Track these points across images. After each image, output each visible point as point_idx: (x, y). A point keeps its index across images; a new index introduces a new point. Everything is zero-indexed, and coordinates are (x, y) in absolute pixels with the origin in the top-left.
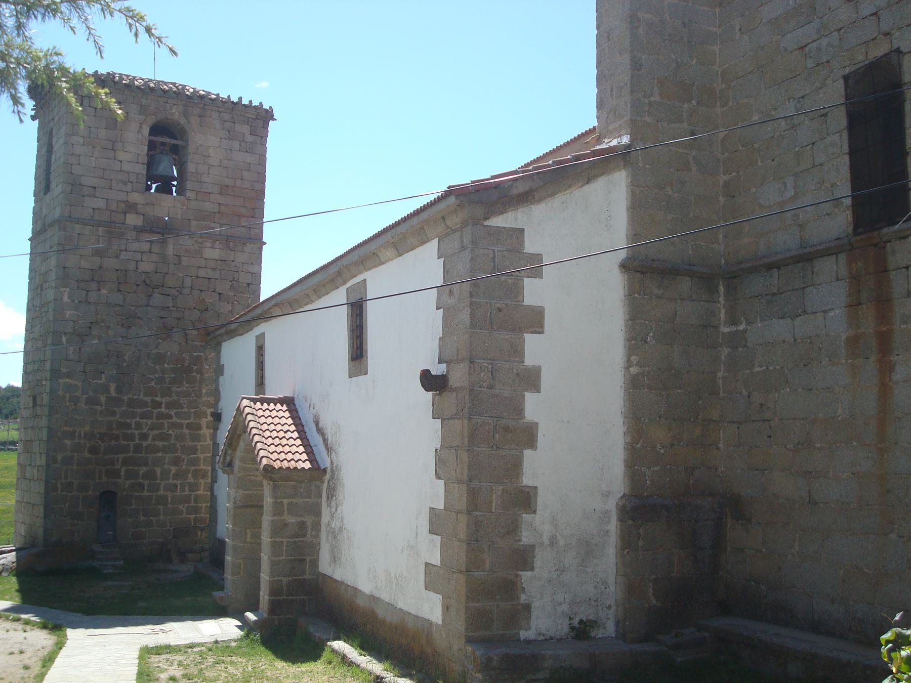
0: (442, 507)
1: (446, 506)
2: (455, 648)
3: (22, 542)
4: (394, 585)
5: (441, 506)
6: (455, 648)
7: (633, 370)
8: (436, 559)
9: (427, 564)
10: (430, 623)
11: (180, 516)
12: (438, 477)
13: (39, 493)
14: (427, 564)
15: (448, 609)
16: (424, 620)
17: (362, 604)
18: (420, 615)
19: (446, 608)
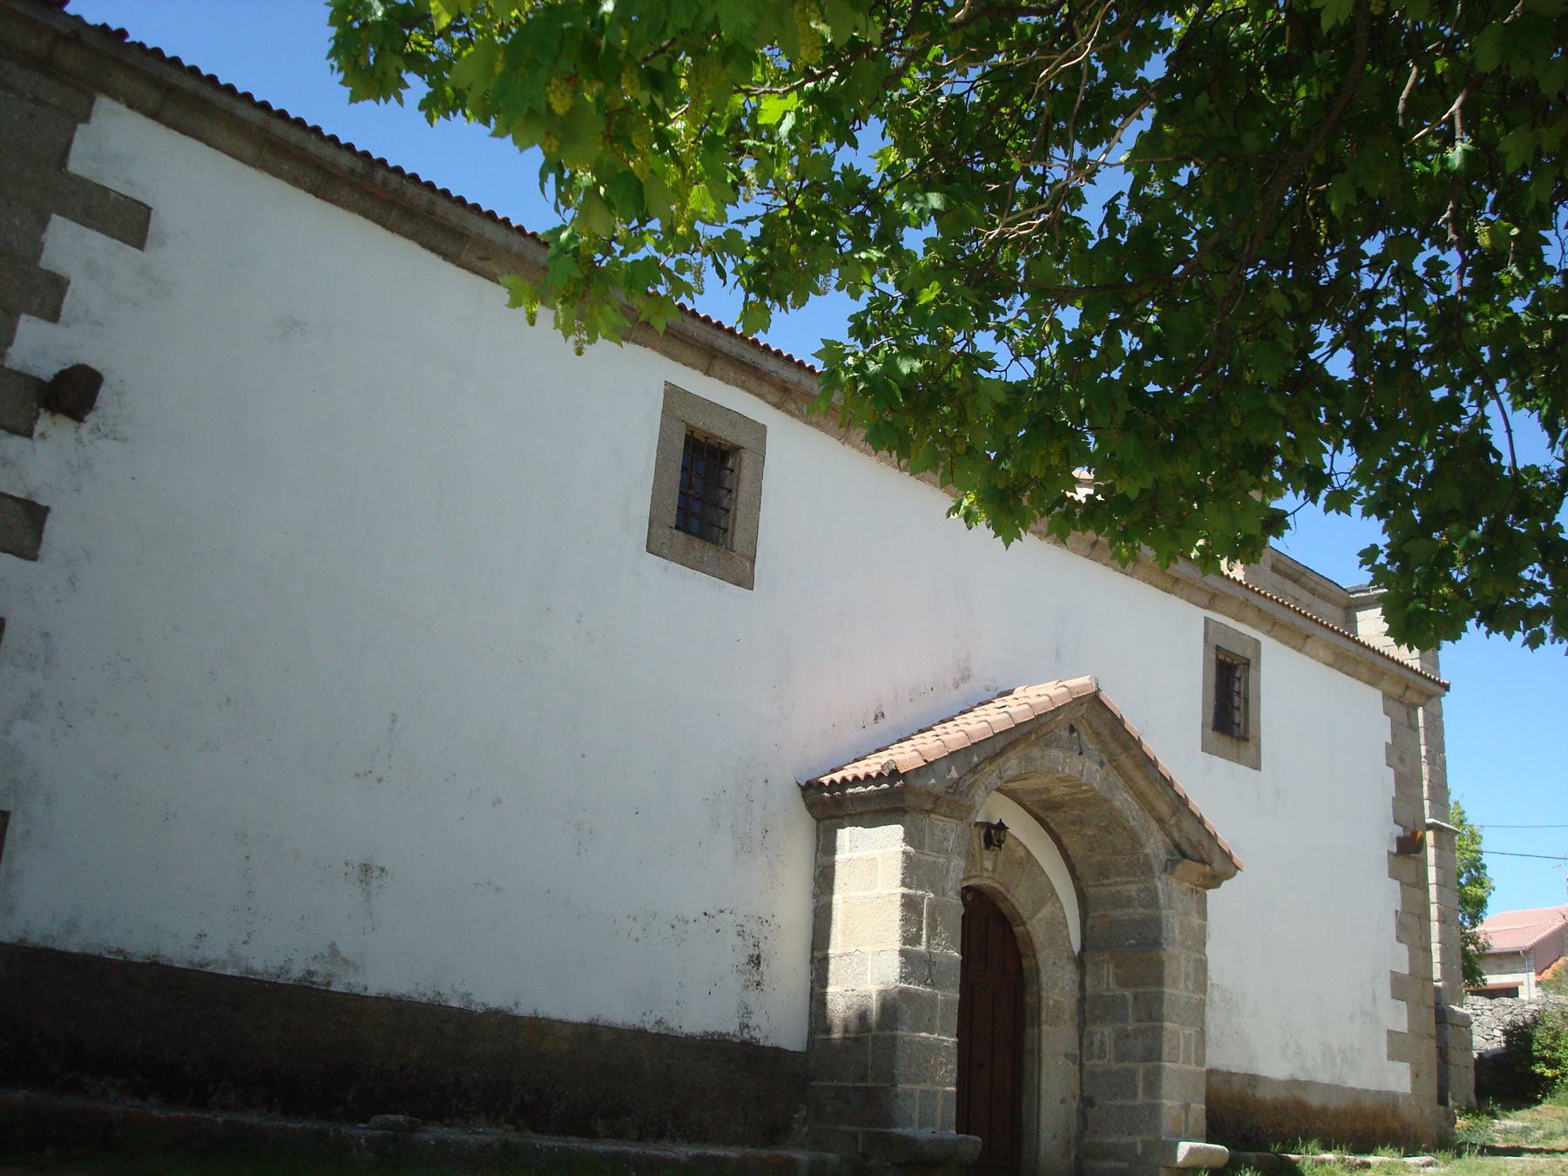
0: (1407, 973)
1: (1075, 848)
2: (1427, 1112)
3: (689, 353)
4: (1338, 1061)
5: (1405, 970)
6: (1427, 1112)
7: (113, 195)
8: (1402, 1026)
9: (1390, 1033)
10: (1395, 1095)
11: (1387, 1159)
12: (1399, 940)
13: (111, 435)
14: (1390, 1033)
15: (1417, 1076)
16: (1388, 1093)
17: (1268, 1097)
18: (1384, 1089)
19: (1416, 1076)
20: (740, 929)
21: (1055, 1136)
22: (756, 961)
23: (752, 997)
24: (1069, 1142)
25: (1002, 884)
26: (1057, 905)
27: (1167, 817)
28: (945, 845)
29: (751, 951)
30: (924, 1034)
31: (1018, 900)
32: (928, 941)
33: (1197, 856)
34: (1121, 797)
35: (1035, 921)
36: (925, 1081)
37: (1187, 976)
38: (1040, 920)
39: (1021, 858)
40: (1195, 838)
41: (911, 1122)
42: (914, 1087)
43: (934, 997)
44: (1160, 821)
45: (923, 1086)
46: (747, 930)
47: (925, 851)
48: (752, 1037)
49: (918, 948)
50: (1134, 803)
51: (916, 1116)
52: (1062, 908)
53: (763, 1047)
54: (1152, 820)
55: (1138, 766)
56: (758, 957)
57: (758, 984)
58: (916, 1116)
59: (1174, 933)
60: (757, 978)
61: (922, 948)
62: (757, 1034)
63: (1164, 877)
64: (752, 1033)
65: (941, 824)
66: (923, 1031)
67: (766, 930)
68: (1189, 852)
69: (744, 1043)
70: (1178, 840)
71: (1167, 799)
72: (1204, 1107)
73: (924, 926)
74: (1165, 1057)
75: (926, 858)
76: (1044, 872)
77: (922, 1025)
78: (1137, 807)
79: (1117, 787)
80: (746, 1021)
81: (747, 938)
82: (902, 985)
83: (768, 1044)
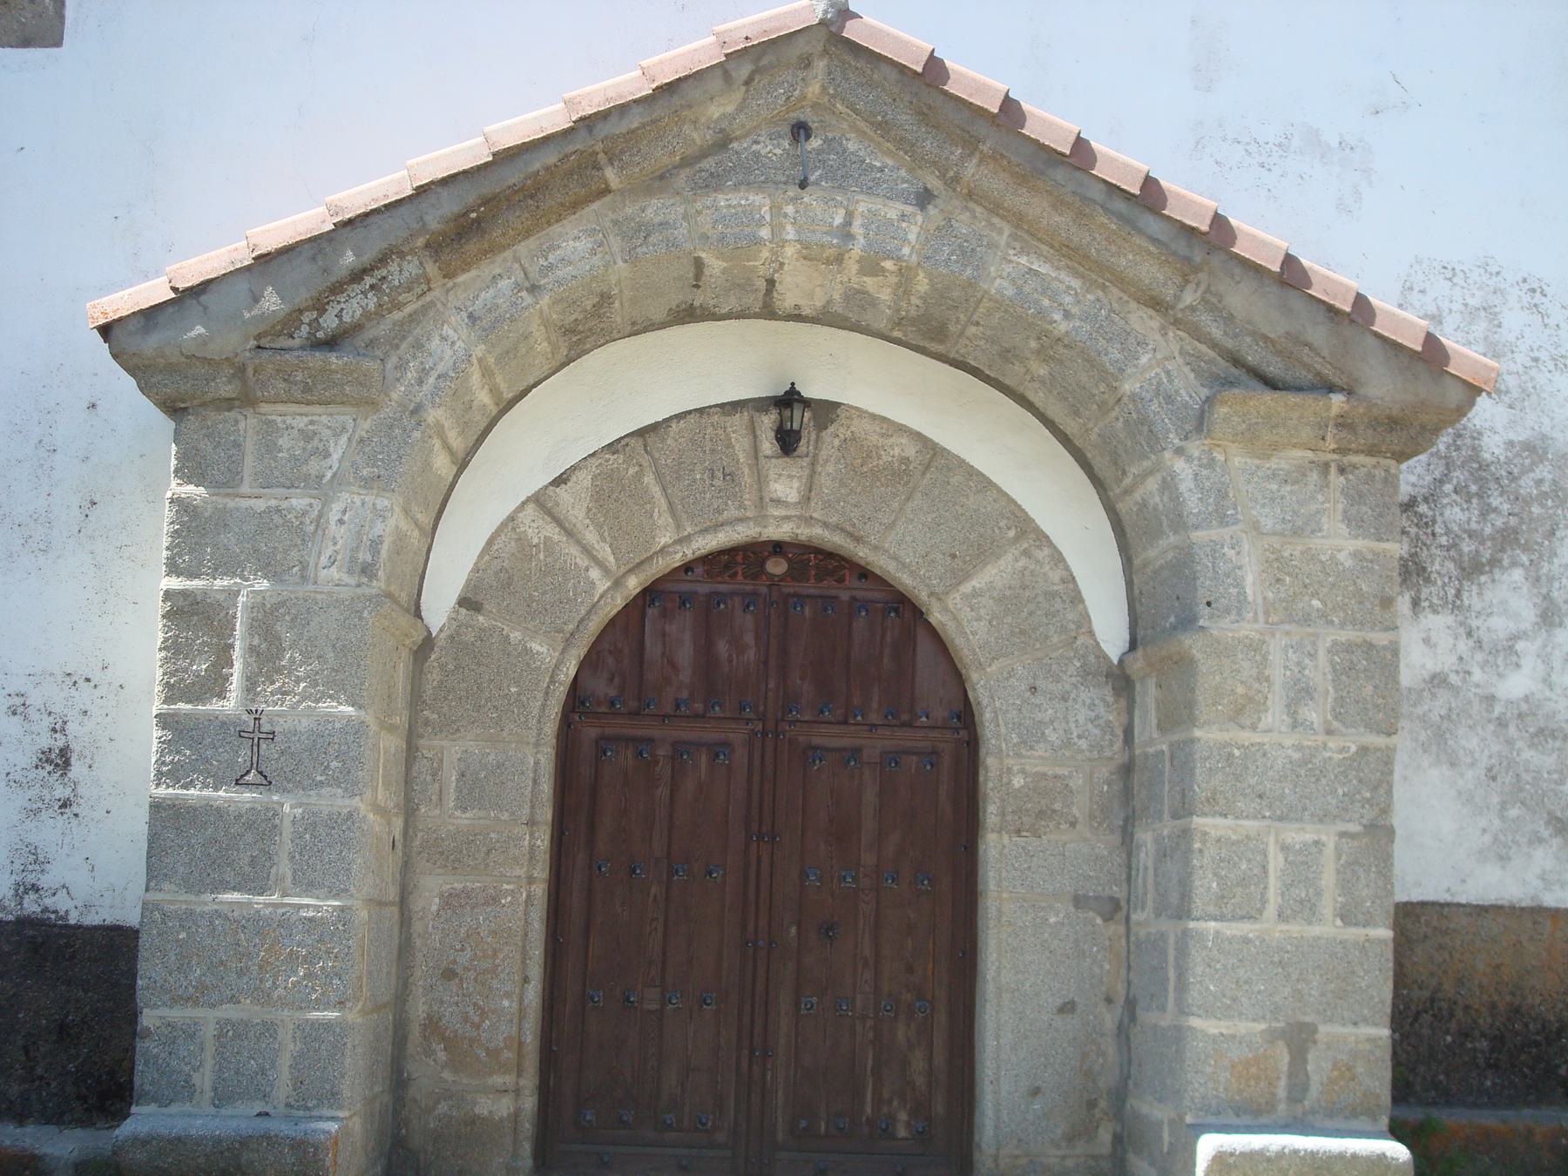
20: (18, 701)
21: (1036, 1092)
22: (60, 760)
23: (48, 832)
24: (1092, 1104)
25: (838, 528)
26: (1043, 554)
27: (1169, 293)
28: (314, 466)
29: (45, 741)
30: (235, 896)
31: (895, 558)
32: (250, 686)
33: (1305, 376)
34: (1008, 268)
35: (955, 600)
36: (234, 1000)
37: (1301, 693)
38: (976, 594)
39: (905, 460)
40: (1276, 326)
41: (187, 1091)
42: (200, 1013)
43: (273, 813)
44: (1156, 304)
45: (229, 1012)
46: (35, 699)
47: (245, 489)
48: (45, 910)
49: (215, 706)
50: (1063, 275)
51: (204, 1080)
52: (1058, 559)
53: (78, 927)
54: (1133, 305)
55: (1022, 179)
56: (65, 752)
57: (65, 804)
58: (204, 1080)
59: (1239, 584)
60: (62, 792)
61: (230, 704)
62: (61, 903)
63: (1195, 448)
64: (48, 902)
65: (301, 422)
66: (234, 889)
67: (84, 695)
68: (1274, 368)
69: (24, 922)
70: (1229, 344)
71: (1145, 244)
72: (1385, 1032)
73: (237, 654)
74: (1199, 903)
75: (245, 503)
76: (990, 482)
77: (229, 876)
78: (1076, 283)
79: (992, 245)
80: (31, 878)
81: (34, 716)
82: (162, 791)
83: (92, 919)
